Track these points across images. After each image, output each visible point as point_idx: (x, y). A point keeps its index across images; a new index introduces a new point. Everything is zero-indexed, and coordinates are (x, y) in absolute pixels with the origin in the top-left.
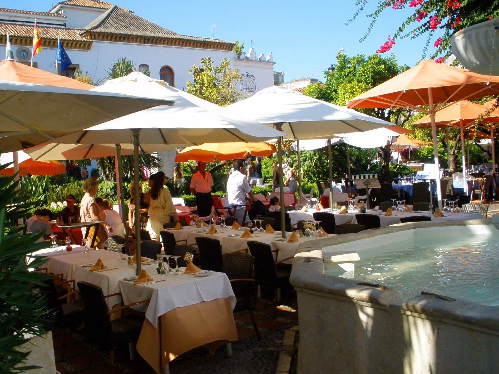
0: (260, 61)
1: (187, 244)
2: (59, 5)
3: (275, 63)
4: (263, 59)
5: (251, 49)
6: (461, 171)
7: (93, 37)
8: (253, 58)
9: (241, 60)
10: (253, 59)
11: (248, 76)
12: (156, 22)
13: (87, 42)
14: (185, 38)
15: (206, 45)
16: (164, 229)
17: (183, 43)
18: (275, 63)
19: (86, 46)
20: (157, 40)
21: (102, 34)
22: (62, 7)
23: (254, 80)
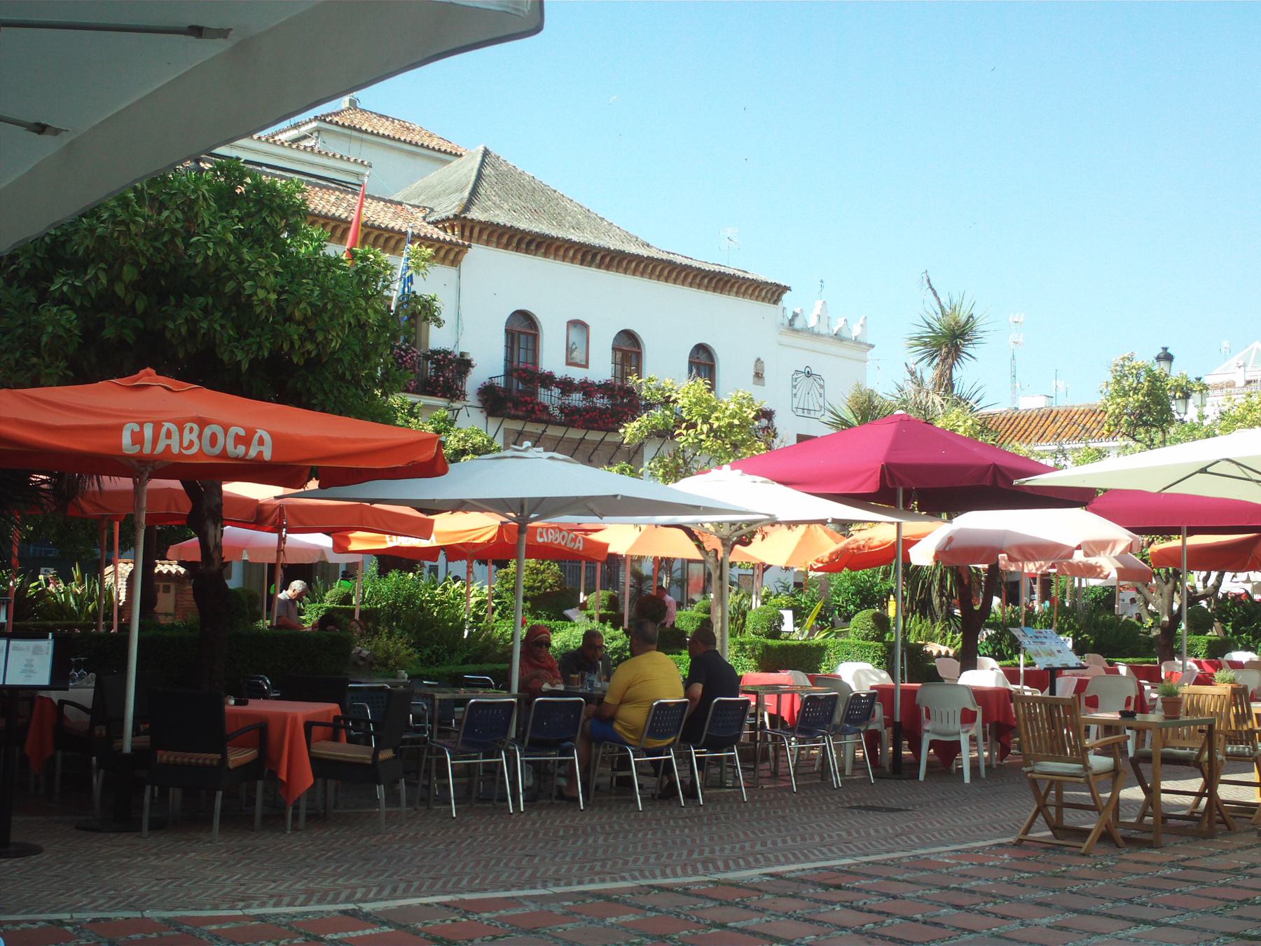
0: (838, 337)
1: (89, 706)
2: (314, 124)
3: (872, 346)
4: (845, 334)
5: (819, 304)
6: (134, 544)
7: (467, 233)
8: (824, 331)
9: (797, 331)
10: (822, 332)
11: (809, 374)
12: (598, 209)
13: (457, 244)
14: (679, 260)
15: (721, 284)
16: (933, 744)
17: (670, 272)
18: (872, 346)
19: (449, 255)
20: (612, 259)
21: (490, 229)
22: (318, 130)
23: (822, 387)
